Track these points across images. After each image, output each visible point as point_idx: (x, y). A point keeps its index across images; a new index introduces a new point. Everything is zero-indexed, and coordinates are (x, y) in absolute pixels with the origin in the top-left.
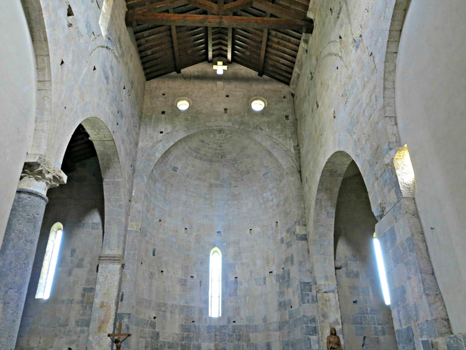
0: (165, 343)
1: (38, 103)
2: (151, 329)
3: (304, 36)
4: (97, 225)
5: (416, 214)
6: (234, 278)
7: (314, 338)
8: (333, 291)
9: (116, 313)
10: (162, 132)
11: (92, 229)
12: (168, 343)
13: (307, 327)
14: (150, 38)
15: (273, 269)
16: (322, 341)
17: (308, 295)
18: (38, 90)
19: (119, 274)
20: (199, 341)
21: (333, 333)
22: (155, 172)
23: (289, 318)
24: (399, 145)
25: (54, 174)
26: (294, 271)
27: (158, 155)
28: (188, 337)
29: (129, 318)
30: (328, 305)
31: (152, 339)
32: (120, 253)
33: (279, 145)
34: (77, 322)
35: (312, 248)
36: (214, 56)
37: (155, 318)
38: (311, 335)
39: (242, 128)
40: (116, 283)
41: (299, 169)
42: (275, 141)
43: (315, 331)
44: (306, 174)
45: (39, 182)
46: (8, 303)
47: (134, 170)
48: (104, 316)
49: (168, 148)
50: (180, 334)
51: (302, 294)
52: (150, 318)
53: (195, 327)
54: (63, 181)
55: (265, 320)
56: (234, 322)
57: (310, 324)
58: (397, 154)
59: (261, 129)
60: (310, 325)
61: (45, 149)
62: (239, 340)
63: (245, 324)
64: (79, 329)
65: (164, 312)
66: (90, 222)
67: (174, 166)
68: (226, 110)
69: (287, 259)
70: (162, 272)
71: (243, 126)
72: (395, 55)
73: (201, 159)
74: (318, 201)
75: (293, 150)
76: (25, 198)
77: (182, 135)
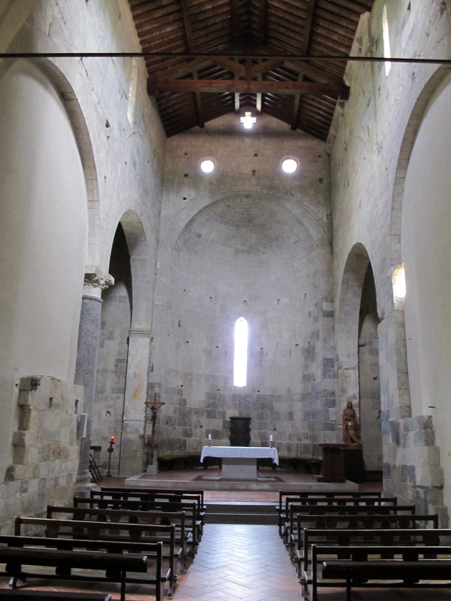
0: (191, 409)
1: (90, 219)
2: (179, 397)
3: (339, 101)
4: (124, 298)
5: (403, 325)
6: (260, 349)
7: (332, 410)
8: (354, 368)
9: (148, 382)
10: (185, 199)
11: (120, 302)
12: (195, 409)
13: (326, 400)
14: (172, 97)
15: (300, 342)
16: (338, 413)
17: (330, 371)
18: (89, 208)
19: (149, 347)
20: (224, 408)
21: (350, 406)
22: (178, 242)
23: (312, 391)
24: (396, 263)
25: (106, 280)
26: (319, 345)
27: (182, 225)
28: (214, 405)
29: (160, 387)
30: (348, 381)
31: (180, 406)
32: (149, 327)
33: (311, 213)
34: (113, 389)
35: (337, 326)
36: (241, 106)
37: (182, 386)
38: (329, 407)
39: (271, 193)
40: (147, 356)
41: (330, 240)
42: (306, 208)
43: (333, 404)
44: (336, 250)
45: (96, 288)
46: (86, 385)
47: (158, 240)
48: (137, 385)
49: (193, 216)
50: (206, 401)
51: (324, 369)
52: (177, 387)
53: (220, 394)
54: (112, 284)
55: (289, 391)
56: (259, 391)
57: (330, 397)
58: (396, 271)
59: (292, 195)
60: (329, 398)
61: (99, 261)
62: (263, 408)
63: (269, 394)
64: (115, 395)
65: (191, 380)
66: (117, 295)
67: (198, 233)
68: (254, 171)
69: (313, 334)
70: (188, 342)
71: (273, 191)
72: (403, 179)
73: (227, 223)
74: (345, 282)
75: (325, 219)
76: (88, 303)
77: (206, 201)
